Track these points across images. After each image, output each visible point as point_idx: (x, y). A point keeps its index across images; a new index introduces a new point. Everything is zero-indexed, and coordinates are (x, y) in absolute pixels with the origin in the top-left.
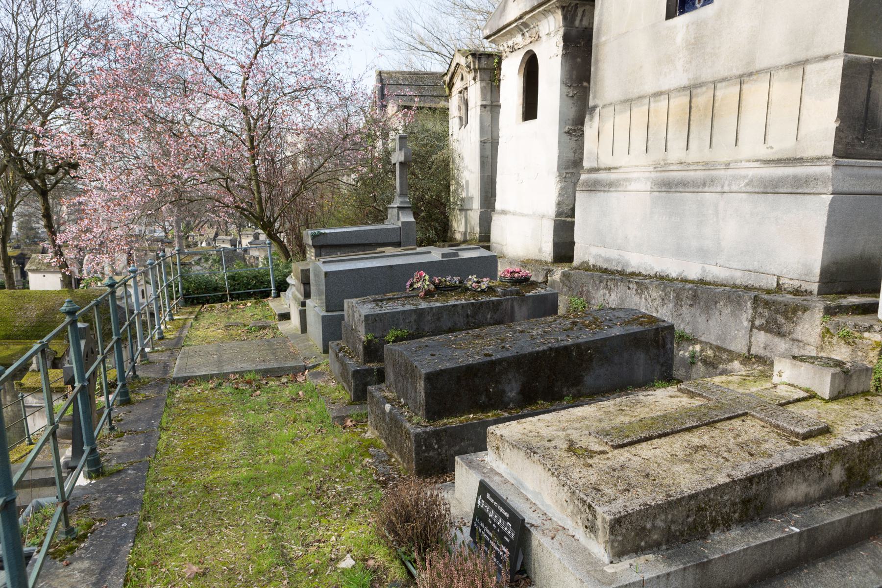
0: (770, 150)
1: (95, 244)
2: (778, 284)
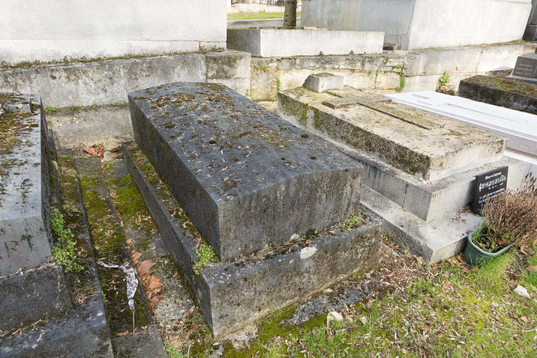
1: (426, 279)
2: (200, 47)
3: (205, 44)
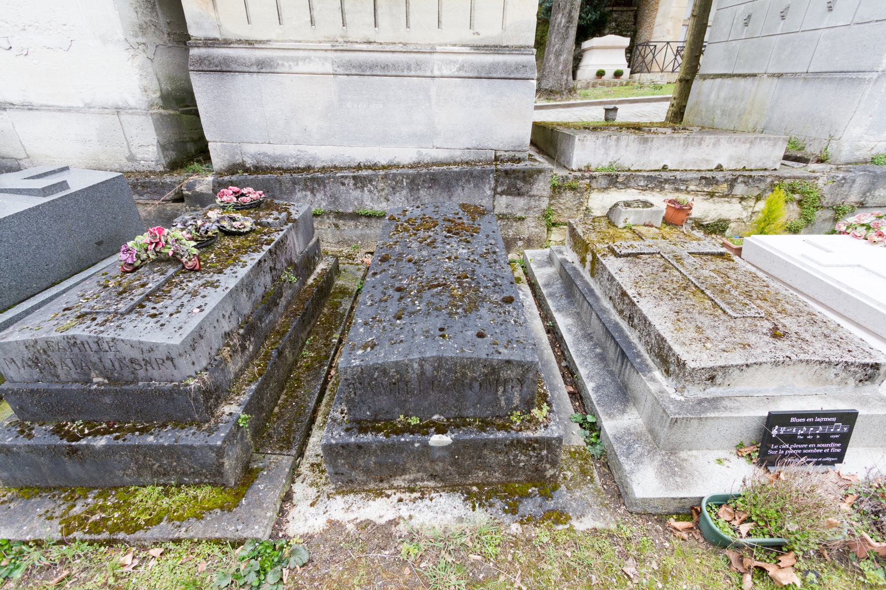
0: (476, 36)
2: (496, 156)
3: (503, 153)
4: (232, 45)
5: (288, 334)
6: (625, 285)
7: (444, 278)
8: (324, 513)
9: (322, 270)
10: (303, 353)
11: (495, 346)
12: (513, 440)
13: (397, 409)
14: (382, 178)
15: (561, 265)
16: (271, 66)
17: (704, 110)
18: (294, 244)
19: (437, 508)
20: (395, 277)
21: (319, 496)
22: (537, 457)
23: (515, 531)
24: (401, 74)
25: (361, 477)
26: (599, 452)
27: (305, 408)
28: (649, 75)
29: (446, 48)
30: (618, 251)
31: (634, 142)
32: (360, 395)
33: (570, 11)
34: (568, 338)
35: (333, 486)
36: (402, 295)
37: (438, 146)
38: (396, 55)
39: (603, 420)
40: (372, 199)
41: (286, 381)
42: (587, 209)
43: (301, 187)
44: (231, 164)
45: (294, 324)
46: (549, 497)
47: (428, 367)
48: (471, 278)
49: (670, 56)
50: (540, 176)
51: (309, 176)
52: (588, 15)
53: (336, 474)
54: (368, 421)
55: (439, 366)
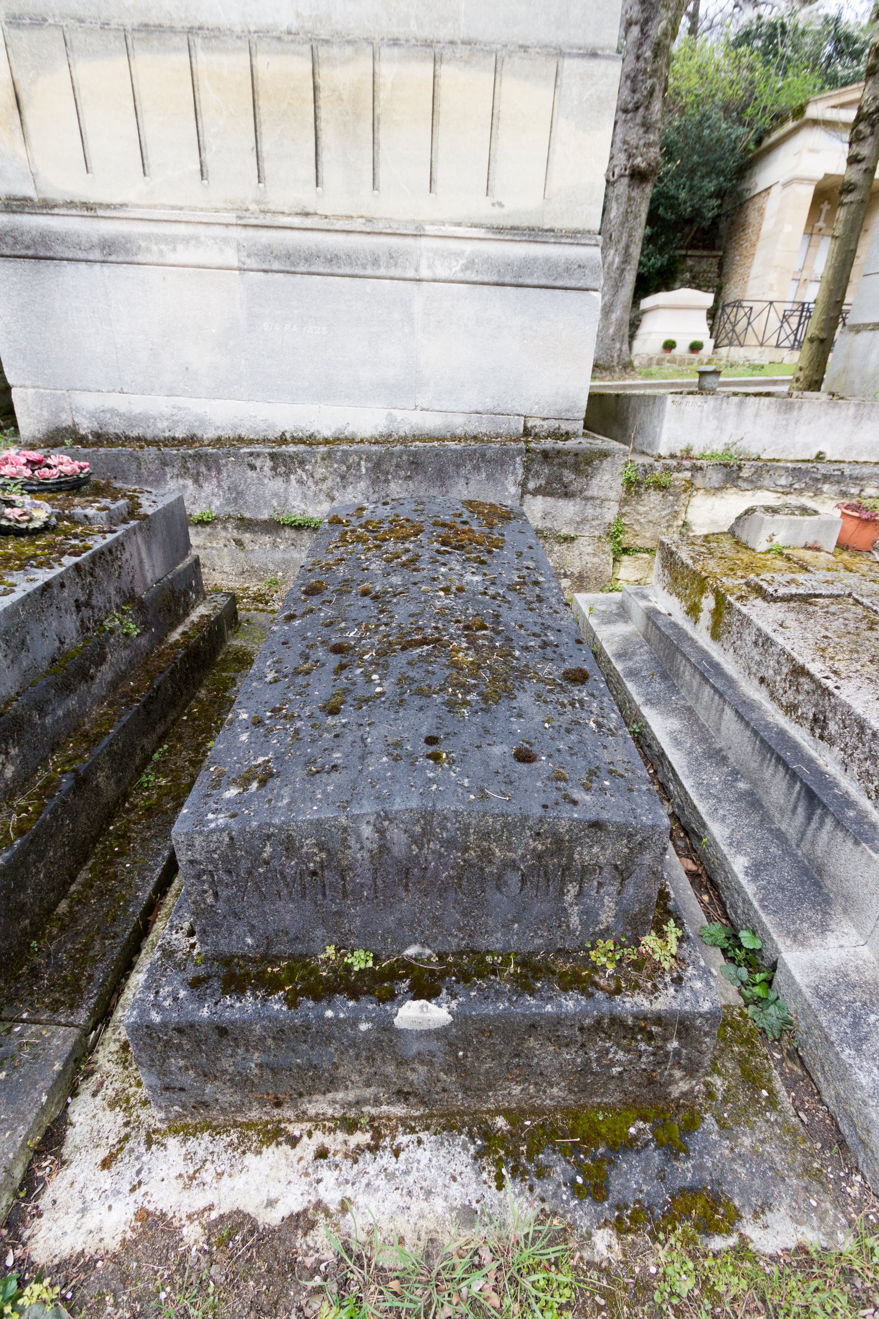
0: (497, 210)
2: (525, 428)
3: (538, 422)
4: (56, 211)
5: (106, 739)
6: (800, 654)
7: (436, 628)
8: (133, 1190)
9: (202, 617)
10: (144, 778)
11: (561, 784)
12: (602, 1018)
13: (320, 932)
14: (323, 459)
15: (649, 618)
16: (127, 251)
17: (858, 381)
18: (141, 562)
19: (410, 1179)
20: (331, 623)
21: (127, 1138)
22: (654, 1054)
23: (605, 1252)
24: (360, 272)
25: (228, 1096)
26: (777, 1024)
27: (128, 902)
28: (742, 349)
29: (443, 228)
30: (771, 590)
31: (768, 408)
32: (228, 900)
33: (627, 247)
34: (676, 758)
35: (162, 1115)
36: (344, 661)
37: (425, 406)
38: (353, 238)
39: (781, 947)
40: (305, 496)
41: (95, 841)
42: (685, 524)
43: (176, 471)
44: (53, 427)
45: (125, 718)
46: (680, 1150)
47: (397, 835)
48: (493, 630)
49: (774, 323)
50: (605, 462)
51: (191, 452)
52: (649, 260)
53: (167, 1089)
54: (250, 960)
55: (424, 833)
